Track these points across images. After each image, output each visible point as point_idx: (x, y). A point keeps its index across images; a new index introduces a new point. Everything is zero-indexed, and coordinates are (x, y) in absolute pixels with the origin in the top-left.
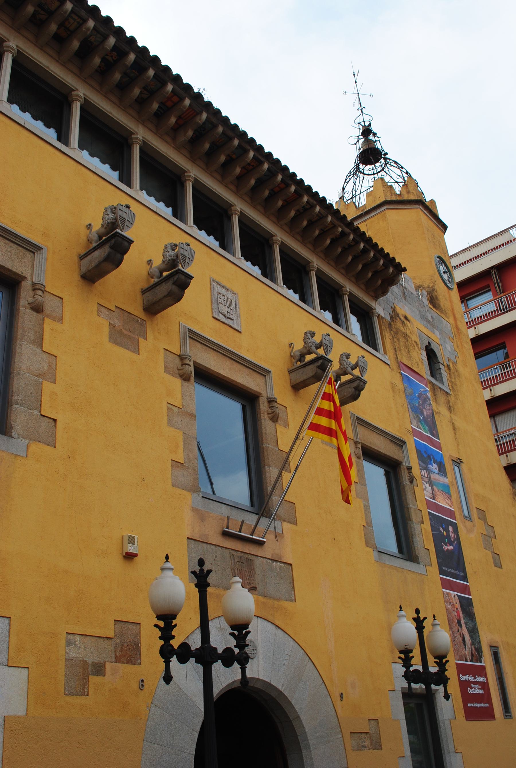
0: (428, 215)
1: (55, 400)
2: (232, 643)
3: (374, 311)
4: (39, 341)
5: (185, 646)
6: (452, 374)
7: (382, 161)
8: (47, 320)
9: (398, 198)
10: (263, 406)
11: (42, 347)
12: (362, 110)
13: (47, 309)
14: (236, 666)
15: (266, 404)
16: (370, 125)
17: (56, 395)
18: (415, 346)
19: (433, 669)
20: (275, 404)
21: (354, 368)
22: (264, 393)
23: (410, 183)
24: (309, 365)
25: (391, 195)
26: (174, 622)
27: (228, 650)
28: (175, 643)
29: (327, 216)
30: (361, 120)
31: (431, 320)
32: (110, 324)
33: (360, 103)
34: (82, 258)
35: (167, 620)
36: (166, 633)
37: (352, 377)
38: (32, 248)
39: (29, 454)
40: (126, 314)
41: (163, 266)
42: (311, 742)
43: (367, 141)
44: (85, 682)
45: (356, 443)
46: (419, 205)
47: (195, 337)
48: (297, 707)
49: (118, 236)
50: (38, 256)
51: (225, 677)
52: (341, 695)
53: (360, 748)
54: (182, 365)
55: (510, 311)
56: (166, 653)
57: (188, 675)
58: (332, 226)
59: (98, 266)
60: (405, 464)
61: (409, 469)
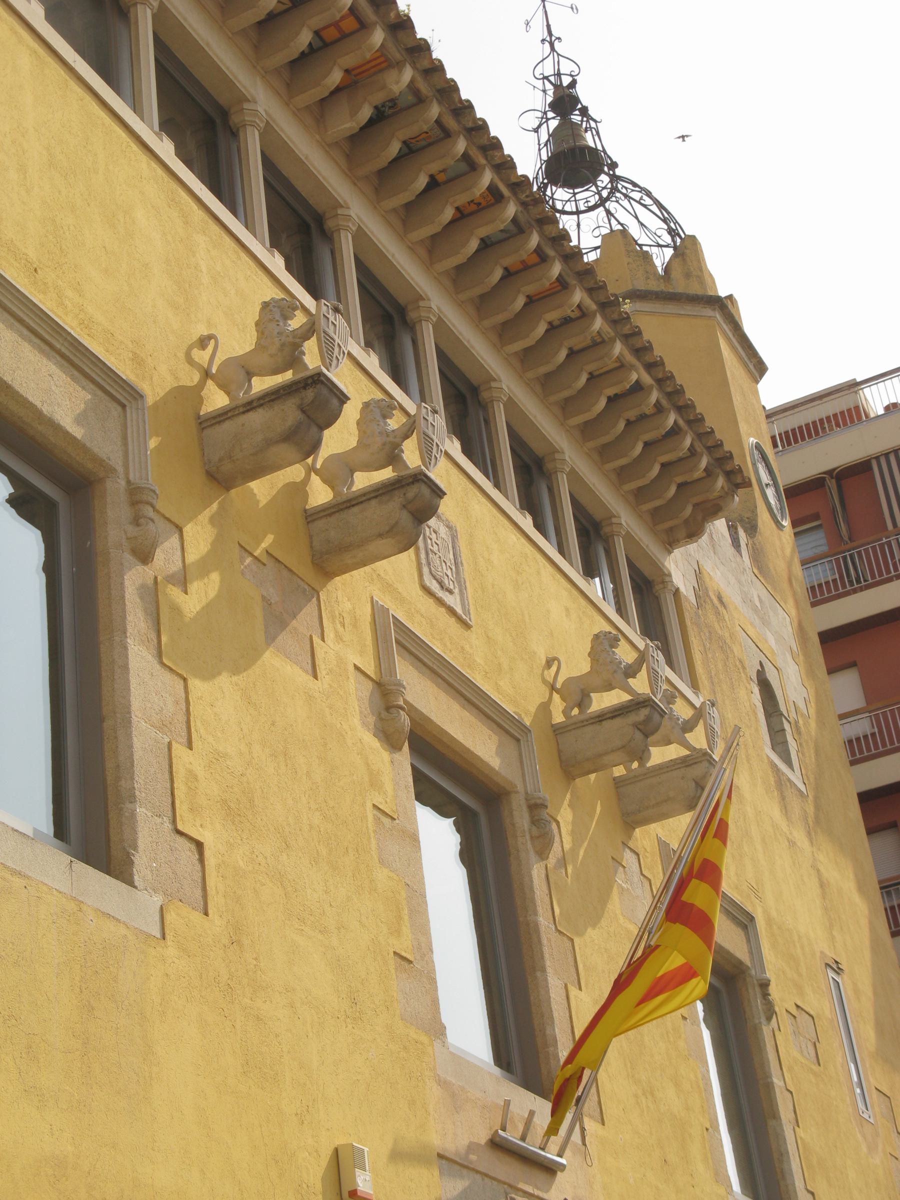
0: (730, 335)
3: (667, 579)
6: (804, 744)
7: (604, 180)
9: (662, 287)
12: (552, 45)
16: (573, 84)
17: (197, 780)
18: (741, 670)
23: (687, 249)
24: (612, 718)
25: (647, 278)
29: (612, 341)
30: (549, 70)
31: (758, 604)
32: (263, 597)
33: (548, 26)
37: (685, 752)
39: (167, 931)
40: (285, 572)
43: (566, 123)
46: (714, 310)
49: (322, 382)
50: (134, 415)
54: (388, 709)
55: (868, 587)
58: (617, 365)
61: (764, 985)
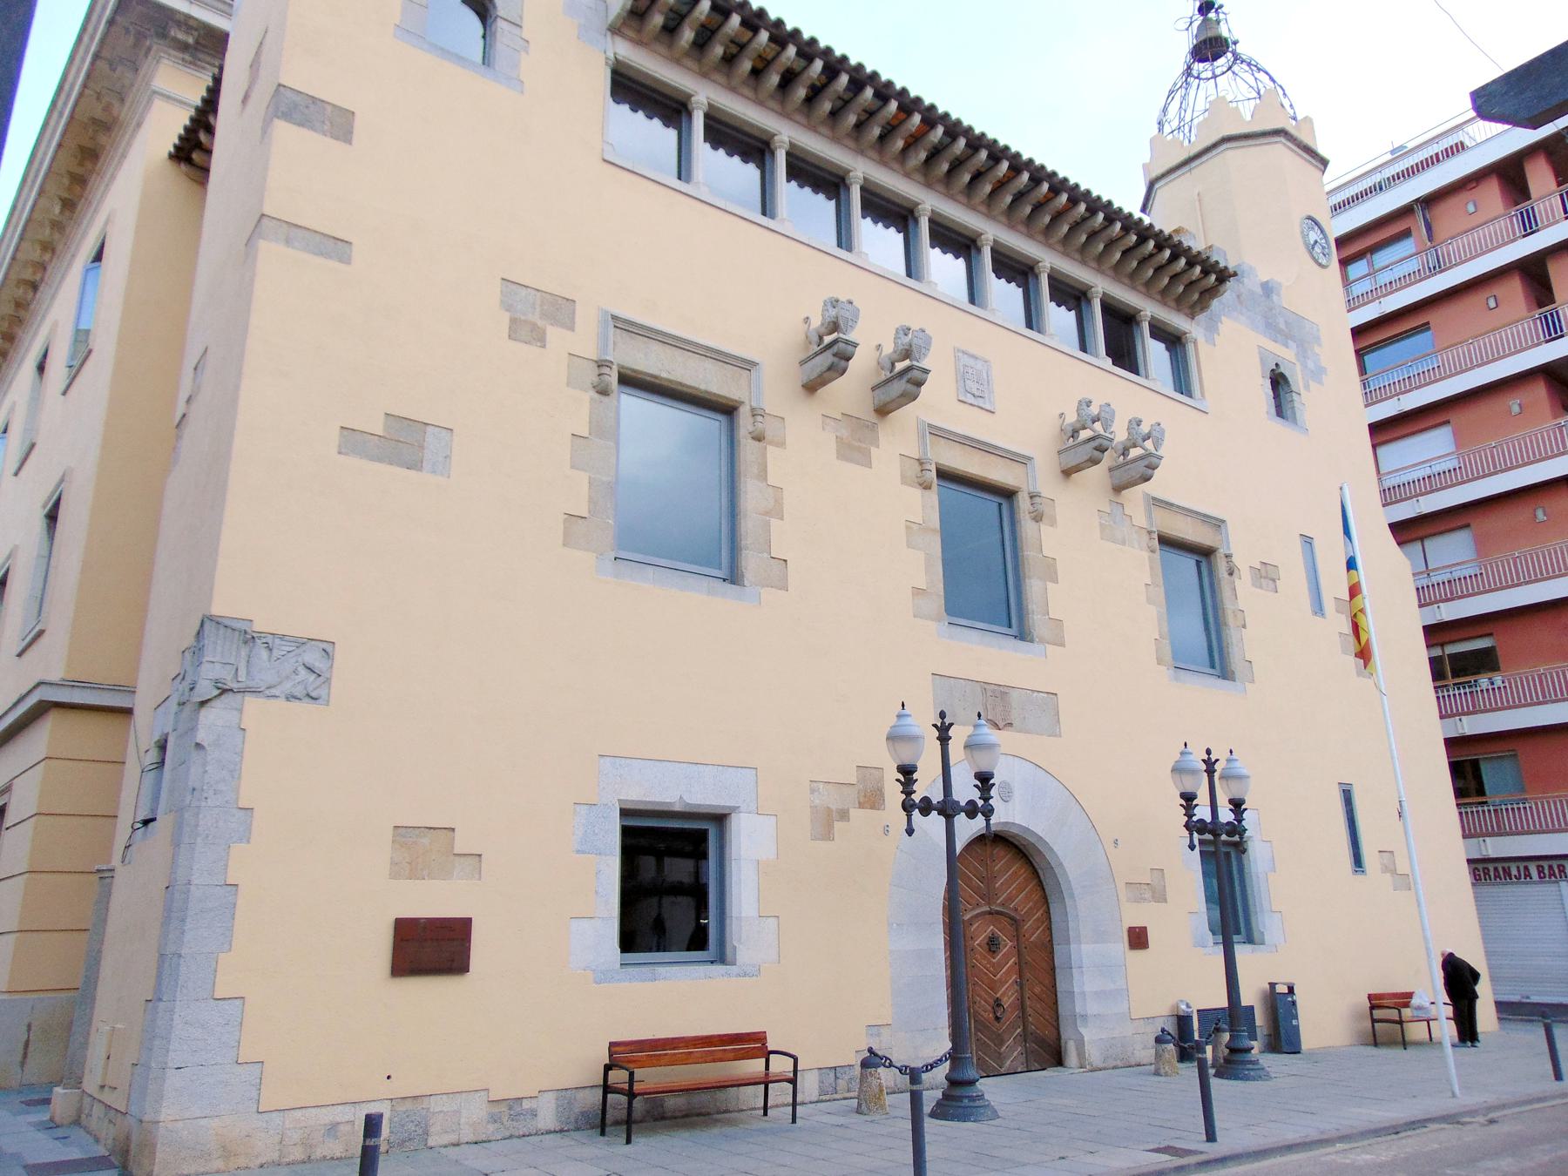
1: (784, 538)
2: (975, 795)
4: (763, 474)
5: (926, 800)
7: (1229, 55)
8: (770, 448)
10: (1023, 502)
11: (765, 479)
13: (769, 435)
14: (980, 818)
15: (1028, 501)
19: (1226, 815)
20: (1037, 500)
21: (1147, 437)
22: (1024, 487)
23: (1271, 92)
26: (915, 776)
27: (971, 803)
28: (916, 798)
34: (803, 363)
35: (907, 771)
36: (908, 791)
38: (748, 365)
41: (895, 356)
42: (1076, 893)
44: (829, 827)
45: (1150, 533)
47: (937, 433)
48: (1060, 854)
51: (968, 828)
52: (1116, 842)
53: (1139, 900)
56: (908, 807)
57: (934, 824)
59: (820, 376)
60: (1222, 551)
